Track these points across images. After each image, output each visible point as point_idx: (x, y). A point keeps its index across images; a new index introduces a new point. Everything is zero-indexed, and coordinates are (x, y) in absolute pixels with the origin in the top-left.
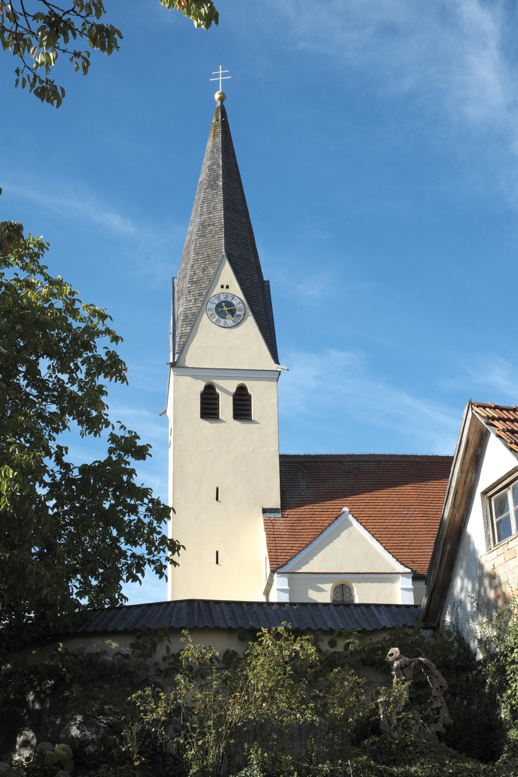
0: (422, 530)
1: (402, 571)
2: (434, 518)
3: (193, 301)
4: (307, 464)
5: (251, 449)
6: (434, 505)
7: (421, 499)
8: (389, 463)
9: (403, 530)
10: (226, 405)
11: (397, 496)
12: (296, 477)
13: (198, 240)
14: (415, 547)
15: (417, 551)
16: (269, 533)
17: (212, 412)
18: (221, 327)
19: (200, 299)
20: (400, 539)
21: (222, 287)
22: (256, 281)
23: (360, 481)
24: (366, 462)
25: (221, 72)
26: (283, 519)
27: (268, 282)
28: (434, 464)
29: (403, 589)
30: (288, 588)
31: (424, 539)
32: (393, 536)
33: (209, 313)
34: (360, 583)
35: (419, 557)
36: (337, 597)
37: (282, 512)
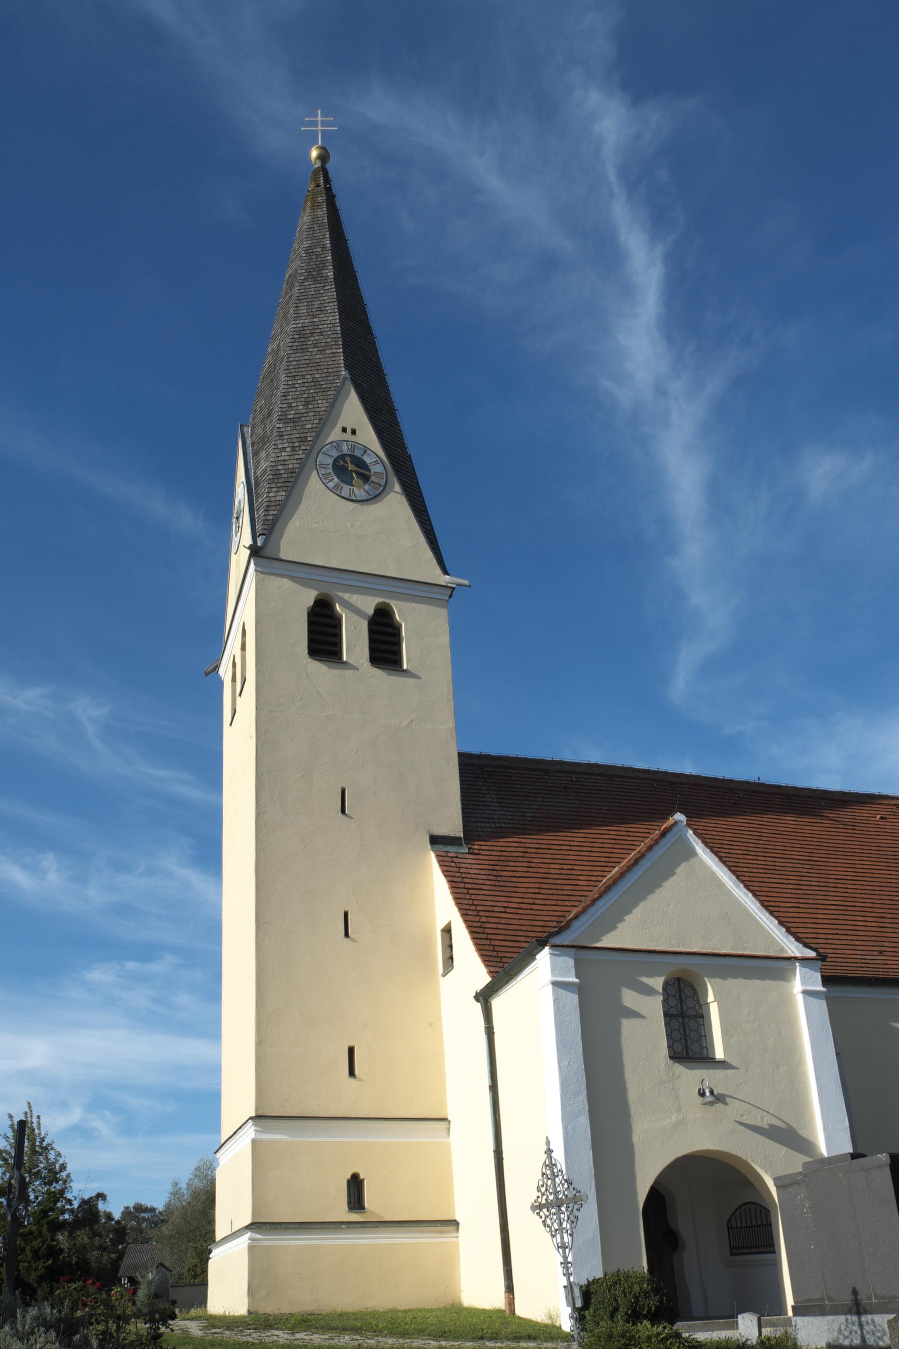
1: (798, 955)
3: (289, 449)
5: (405, 723)
10: (354, 637)
12: (475, 787)
13: (293, 355)
16: (454, 879)
18: (344, 498)
19: (302, 448)
21: (344, 430)
30: (574, 980)
33: (322, 471)
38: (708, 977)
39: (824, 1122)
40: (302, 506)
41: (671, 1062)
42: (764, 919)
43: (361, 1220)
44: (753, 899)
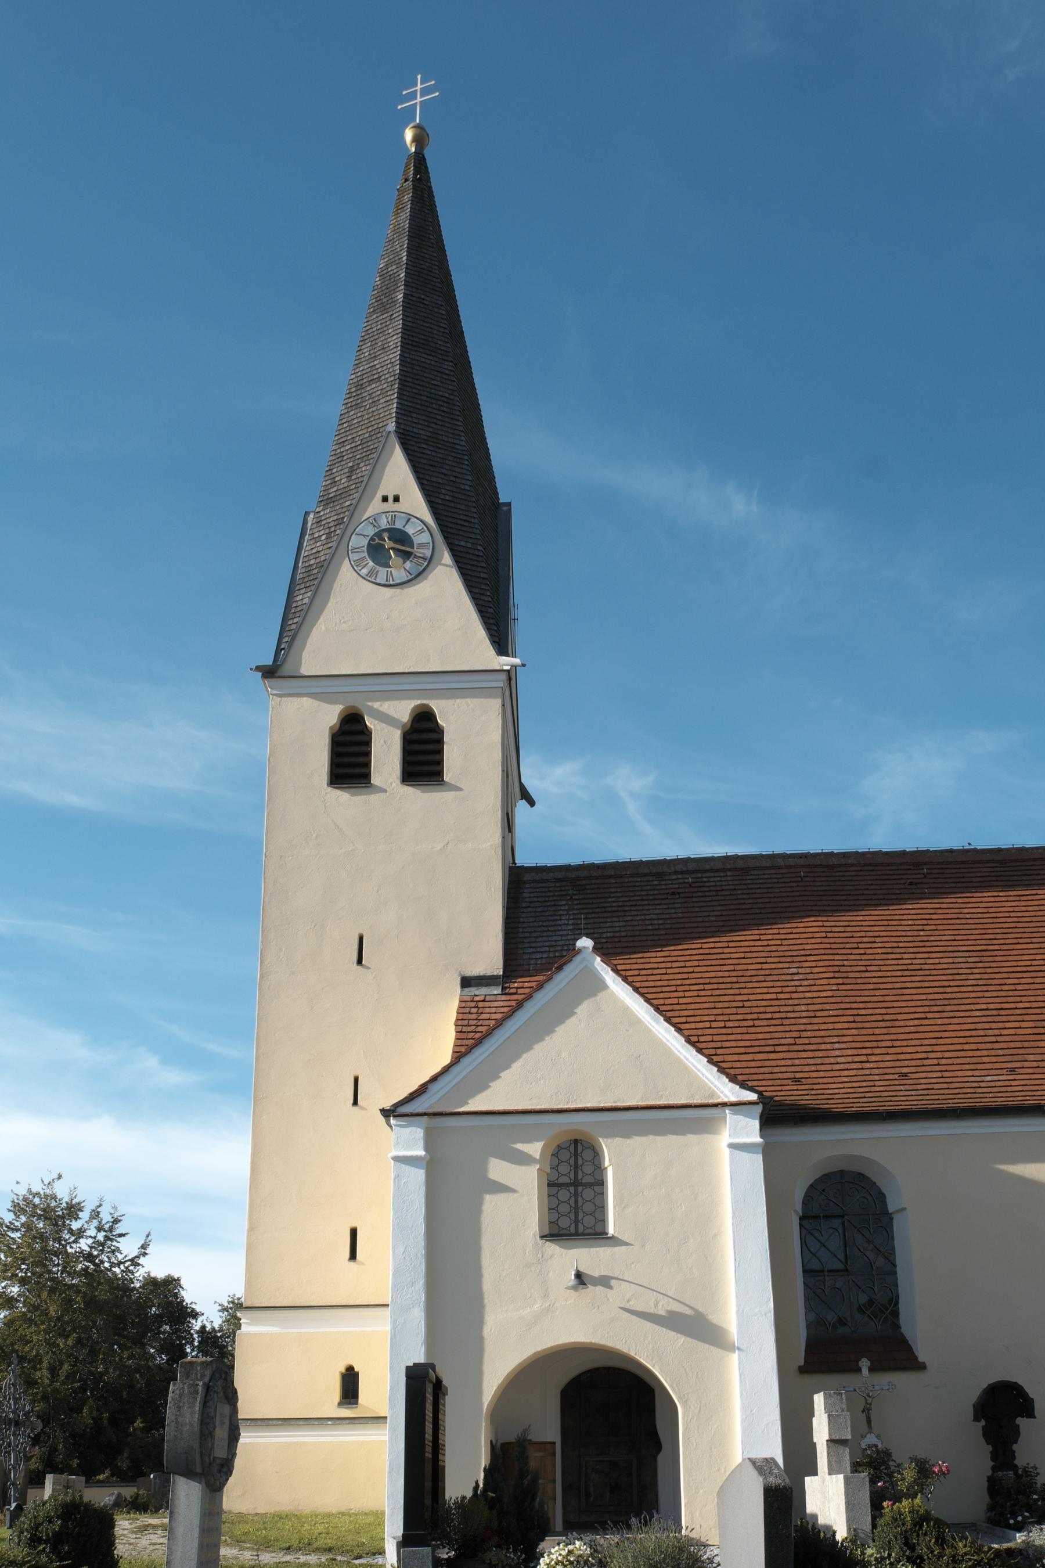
0: (828, 1007)
1: (733, 1099)
2: (859, 981)
4: (584, 882)
6: (862, 951)
7: (832, 940)
8: (767, 872)
9: (782, 1009)
11: (778, 937)
12: (553, 908)
14: (807, 1047)
15: (811, 1054)
16: (465, 1029)
17: (357, 771)
18: (379, 585)
20: (771, 1029)
22: (467, 488)
23: (697, 909)
24: (718, 870)
25: (419, 86)
26: (504, 998)
27: (509, 504)
28: (871, 868)
29: (732, 1146)
31: (831, 1026)
32: (757, 1023)
33: (354, 557)
34: (629, 1137)
35: (813, 1068)
36: (560, 1175)
37: (504, 983)
38: (603, 1137)
39: (739, 1305)
40: (330, 605)
41: (540, 1242)
42: (690, 1058)
43: (352, 1416)
44: (676, 1034)
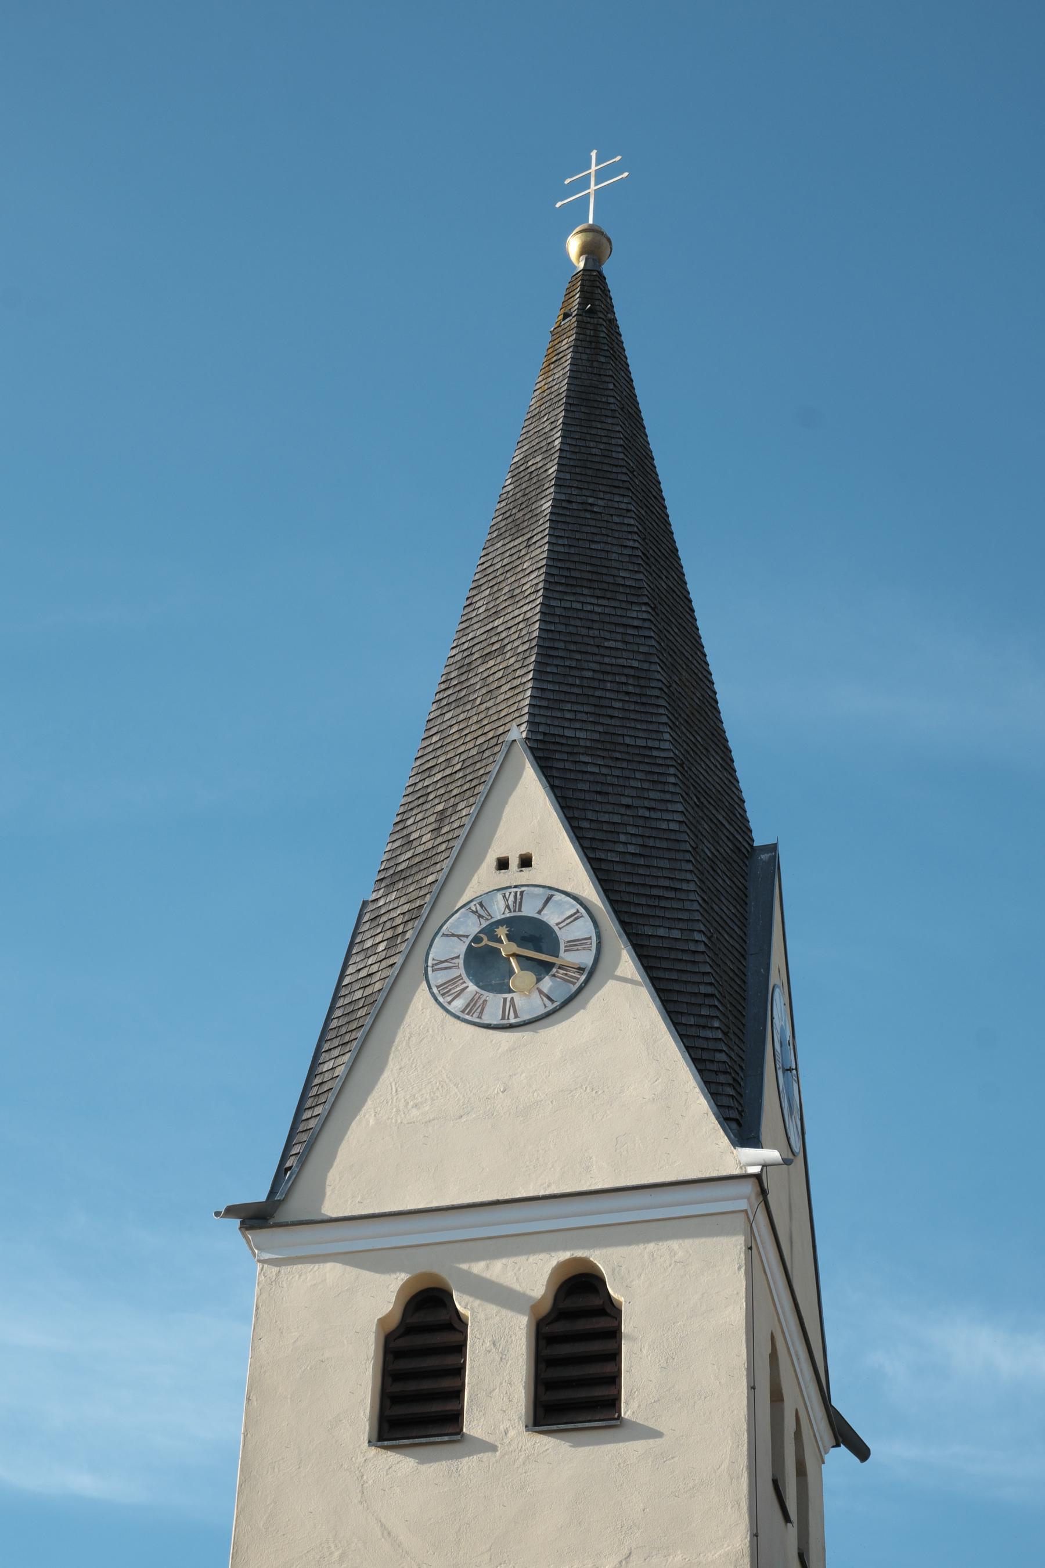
18: (488, 1027)
27: (773, 848)
33: (437, 978)
